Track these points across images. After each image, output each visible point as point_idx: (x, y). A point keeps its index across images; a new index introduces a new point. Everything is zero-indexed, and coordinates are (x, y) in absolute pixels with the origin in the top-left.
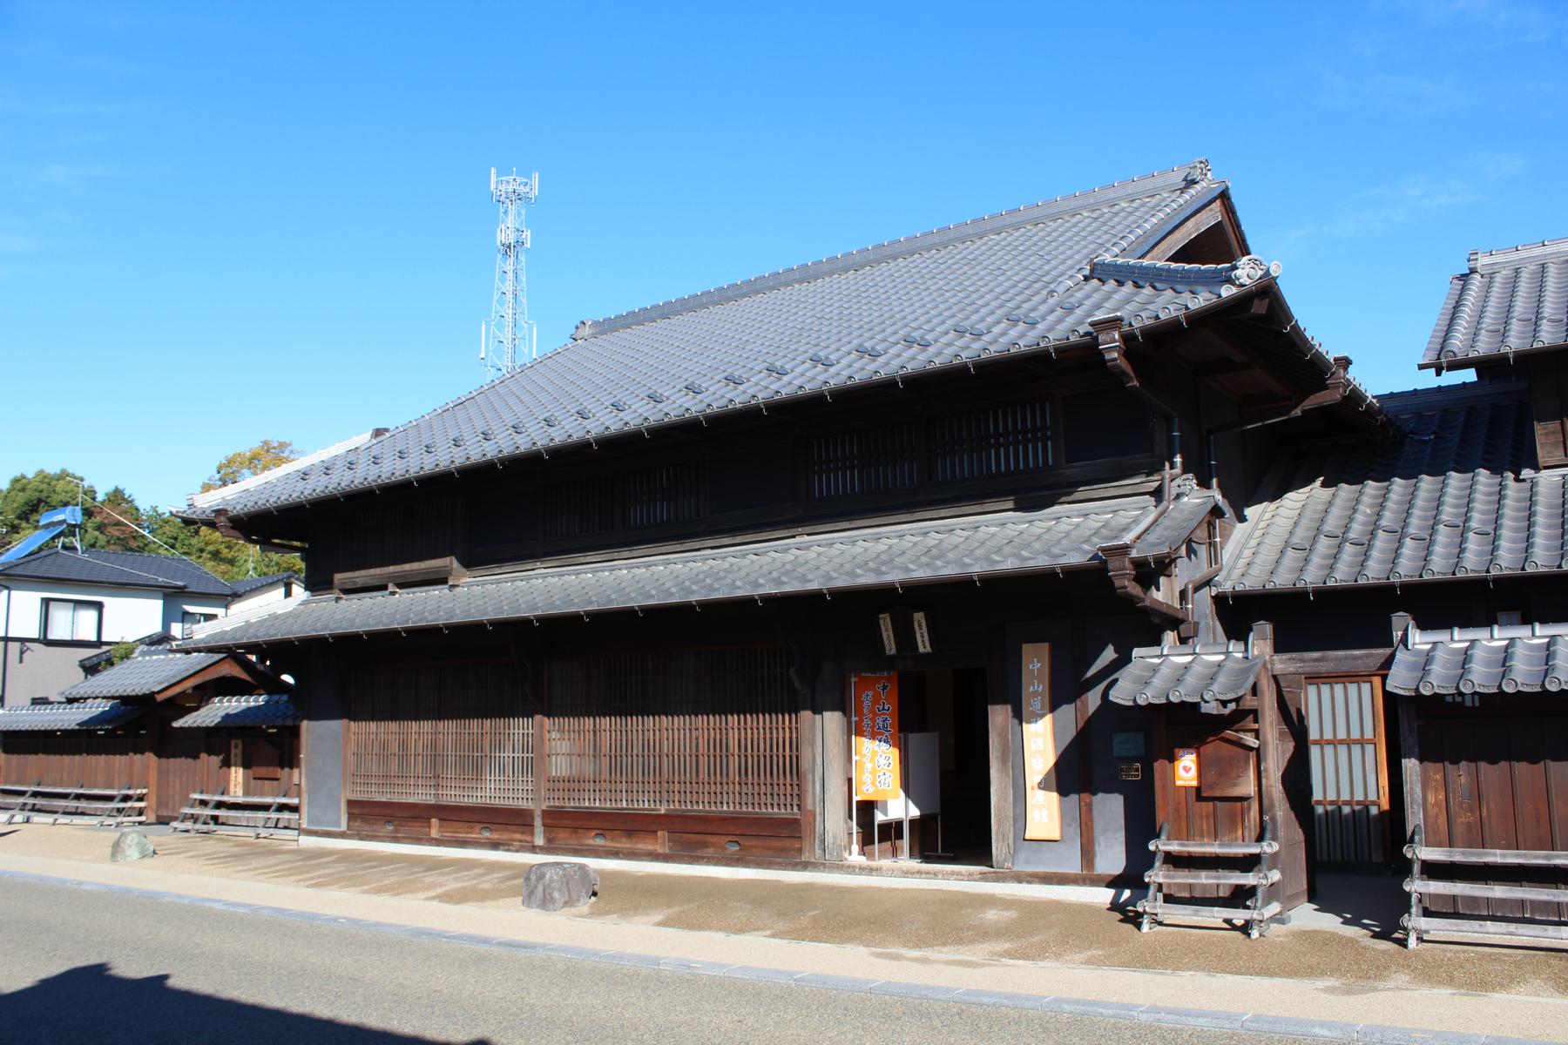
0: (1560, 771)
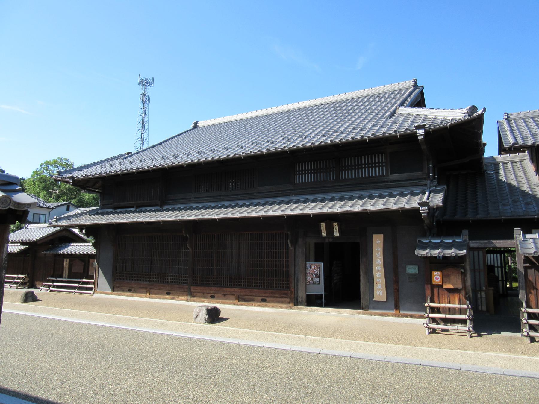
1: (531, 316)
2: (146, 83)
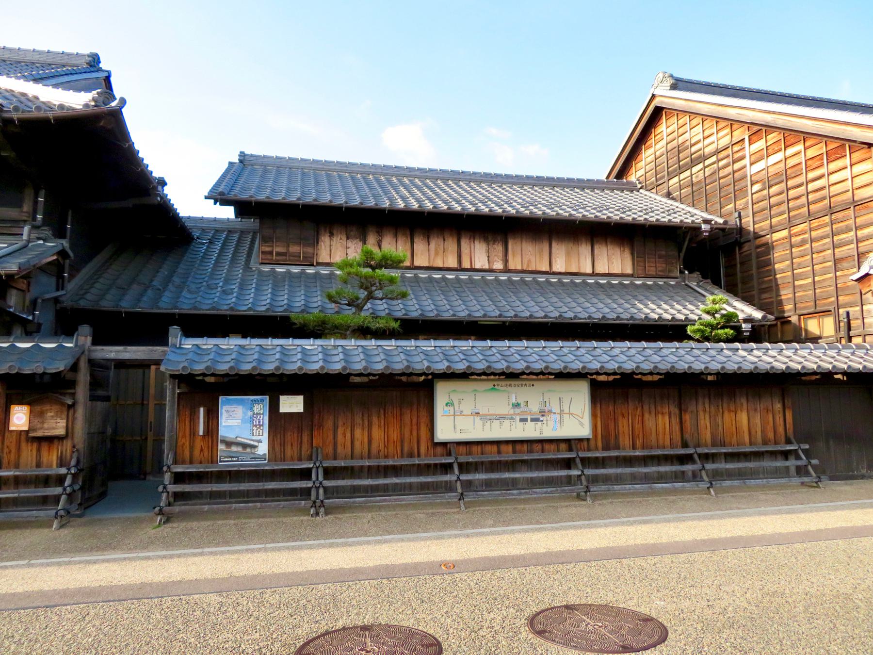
1: (179, 478)
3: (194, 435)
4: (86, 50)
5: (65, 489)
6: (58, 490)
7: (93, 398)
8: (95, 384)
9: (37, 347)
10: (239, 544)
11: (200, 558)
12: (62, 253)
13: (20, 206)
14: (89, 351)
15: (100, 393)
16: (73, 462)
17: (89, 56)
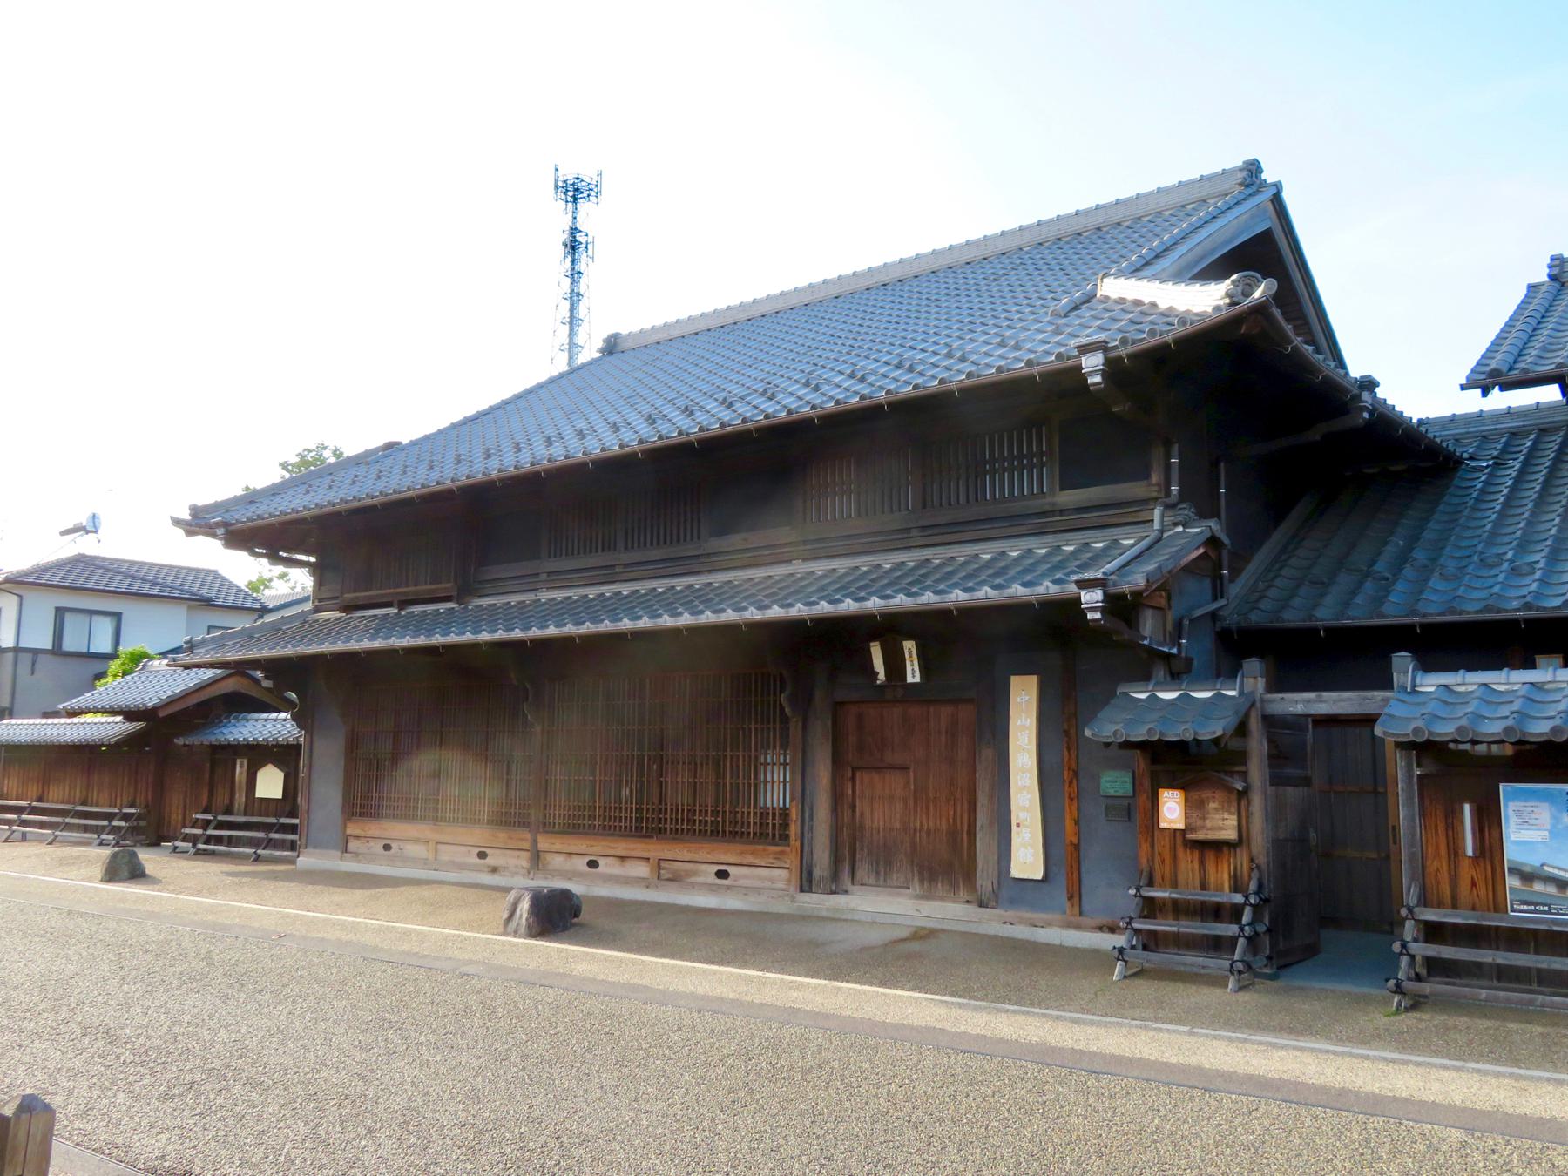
0: (1565, 815)
1: (1433, 932)
2: (574, 192)
3: (1456, 854)
4: (1235, 161)
5: (1242, 930)
6: (1233, 929)
7: (1277, 780)
8: (1278, 757)
9: (1185, 697)
10: (1538, 1067)
11: (1454, 1074)
12: (1213, 542)
13: (1148, 477)
14: (1262, 701)
15: (1290, 771)
16: (1253, 886)
17: (1241, 170)
